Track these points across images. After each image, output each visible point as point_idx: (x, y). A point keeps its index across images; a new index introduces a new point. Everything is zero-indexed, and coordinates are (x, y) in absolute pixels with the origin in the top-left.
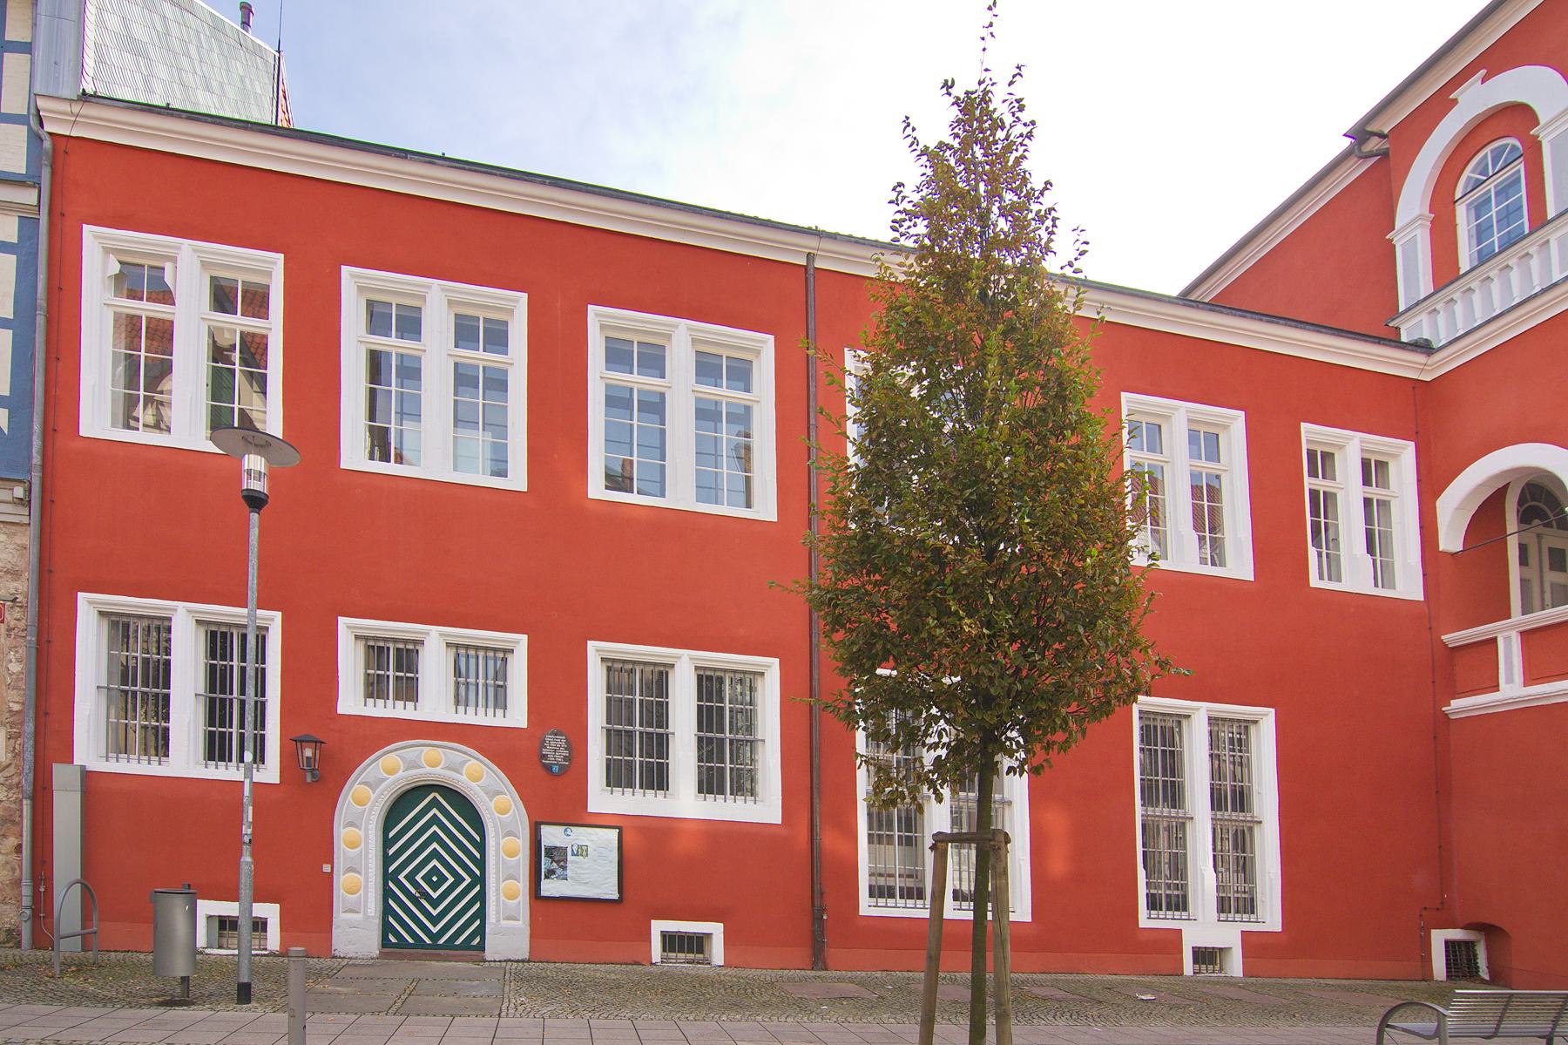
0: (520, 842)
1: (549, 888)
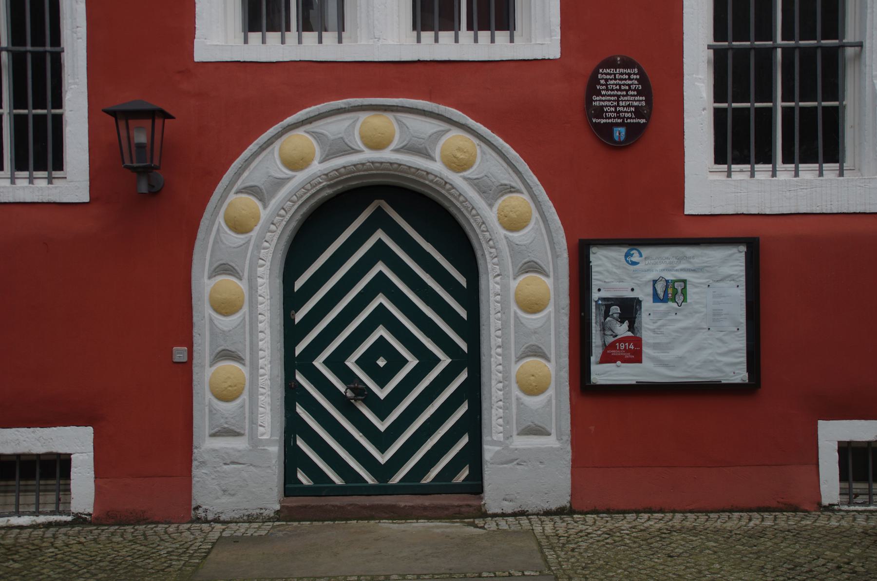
0: (549, 282)
1: (603, 374)
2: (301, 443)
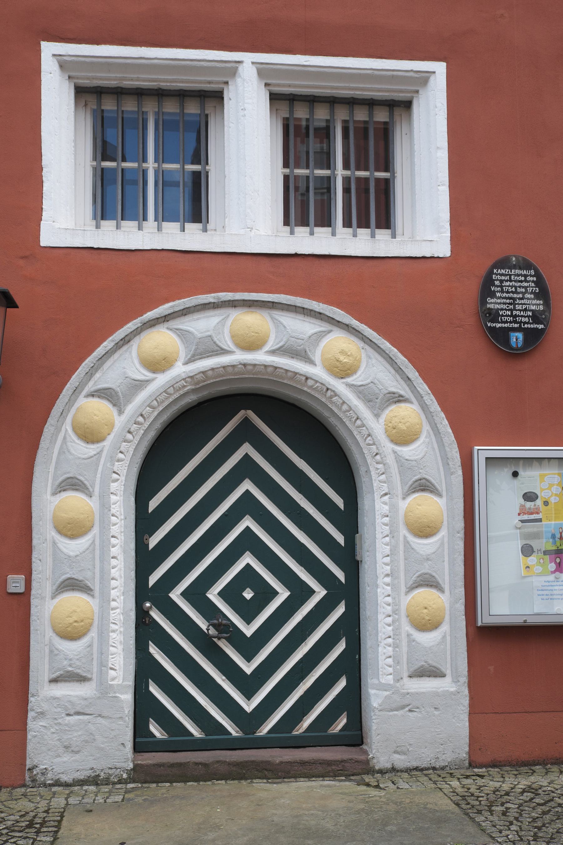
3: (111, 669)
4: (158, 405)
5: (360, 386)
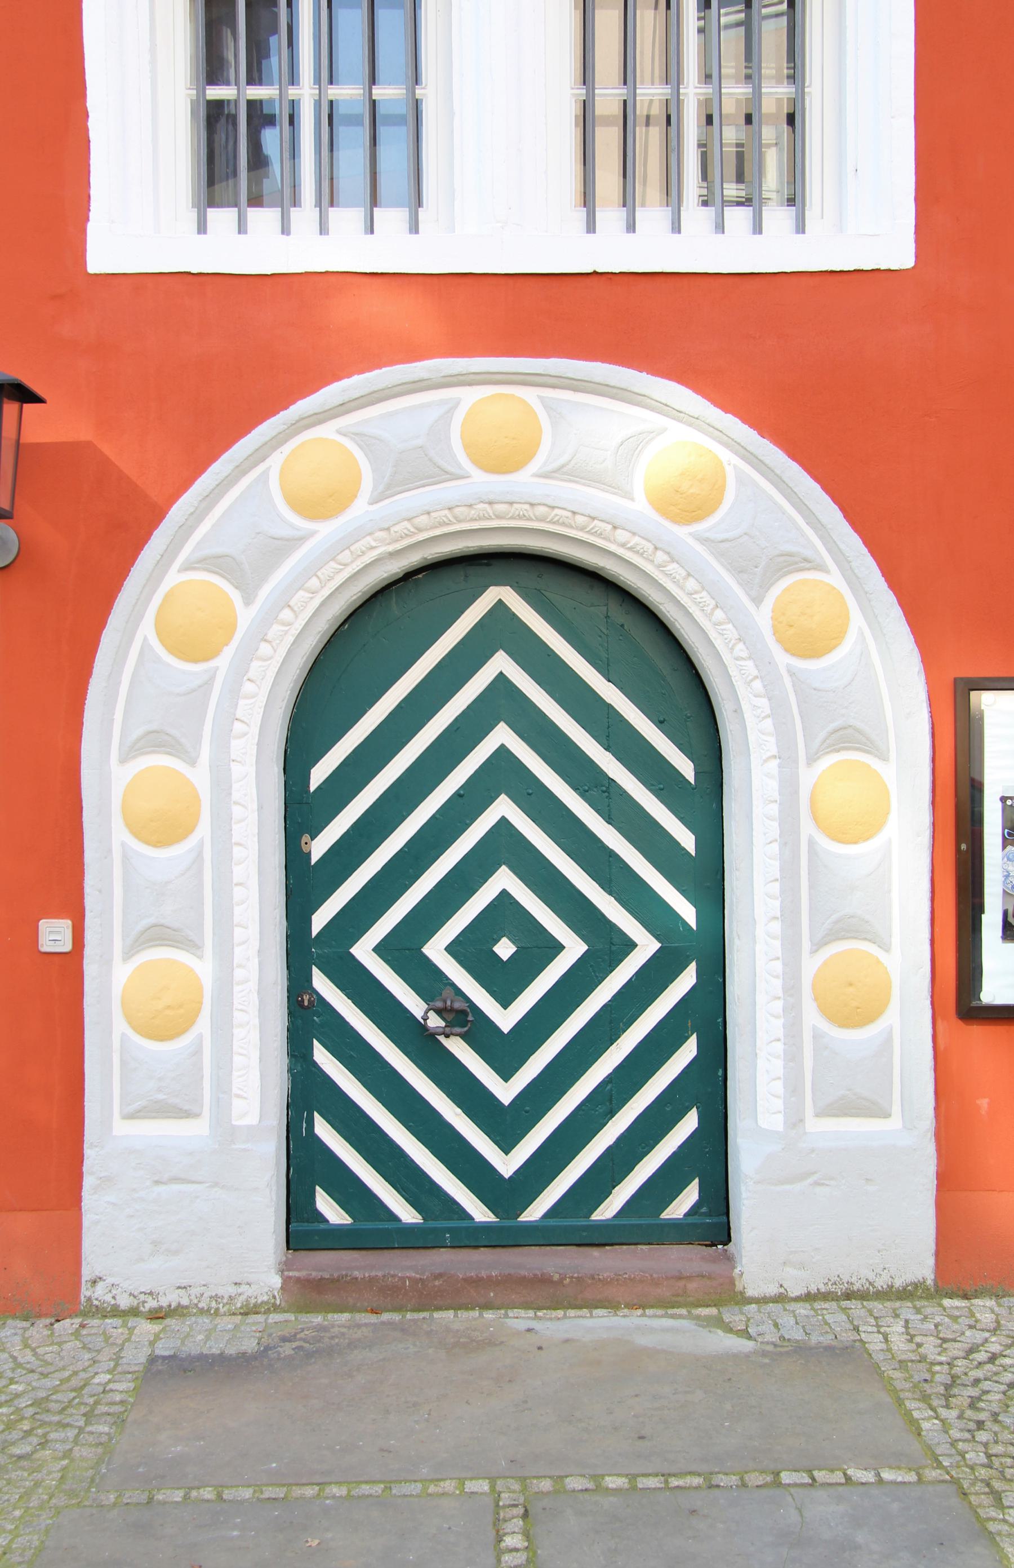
2: (324, 1130)
3: (238, 1096)
4: (275, 651)
5: (722, 541)
